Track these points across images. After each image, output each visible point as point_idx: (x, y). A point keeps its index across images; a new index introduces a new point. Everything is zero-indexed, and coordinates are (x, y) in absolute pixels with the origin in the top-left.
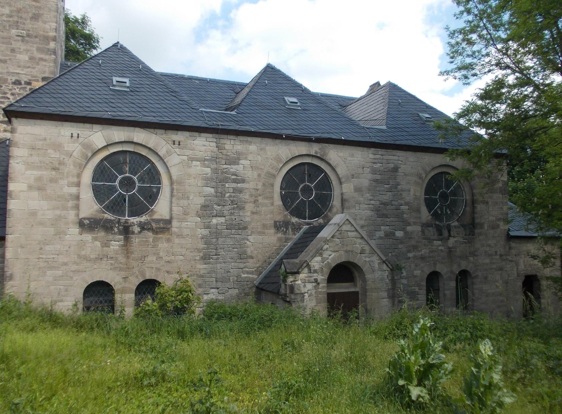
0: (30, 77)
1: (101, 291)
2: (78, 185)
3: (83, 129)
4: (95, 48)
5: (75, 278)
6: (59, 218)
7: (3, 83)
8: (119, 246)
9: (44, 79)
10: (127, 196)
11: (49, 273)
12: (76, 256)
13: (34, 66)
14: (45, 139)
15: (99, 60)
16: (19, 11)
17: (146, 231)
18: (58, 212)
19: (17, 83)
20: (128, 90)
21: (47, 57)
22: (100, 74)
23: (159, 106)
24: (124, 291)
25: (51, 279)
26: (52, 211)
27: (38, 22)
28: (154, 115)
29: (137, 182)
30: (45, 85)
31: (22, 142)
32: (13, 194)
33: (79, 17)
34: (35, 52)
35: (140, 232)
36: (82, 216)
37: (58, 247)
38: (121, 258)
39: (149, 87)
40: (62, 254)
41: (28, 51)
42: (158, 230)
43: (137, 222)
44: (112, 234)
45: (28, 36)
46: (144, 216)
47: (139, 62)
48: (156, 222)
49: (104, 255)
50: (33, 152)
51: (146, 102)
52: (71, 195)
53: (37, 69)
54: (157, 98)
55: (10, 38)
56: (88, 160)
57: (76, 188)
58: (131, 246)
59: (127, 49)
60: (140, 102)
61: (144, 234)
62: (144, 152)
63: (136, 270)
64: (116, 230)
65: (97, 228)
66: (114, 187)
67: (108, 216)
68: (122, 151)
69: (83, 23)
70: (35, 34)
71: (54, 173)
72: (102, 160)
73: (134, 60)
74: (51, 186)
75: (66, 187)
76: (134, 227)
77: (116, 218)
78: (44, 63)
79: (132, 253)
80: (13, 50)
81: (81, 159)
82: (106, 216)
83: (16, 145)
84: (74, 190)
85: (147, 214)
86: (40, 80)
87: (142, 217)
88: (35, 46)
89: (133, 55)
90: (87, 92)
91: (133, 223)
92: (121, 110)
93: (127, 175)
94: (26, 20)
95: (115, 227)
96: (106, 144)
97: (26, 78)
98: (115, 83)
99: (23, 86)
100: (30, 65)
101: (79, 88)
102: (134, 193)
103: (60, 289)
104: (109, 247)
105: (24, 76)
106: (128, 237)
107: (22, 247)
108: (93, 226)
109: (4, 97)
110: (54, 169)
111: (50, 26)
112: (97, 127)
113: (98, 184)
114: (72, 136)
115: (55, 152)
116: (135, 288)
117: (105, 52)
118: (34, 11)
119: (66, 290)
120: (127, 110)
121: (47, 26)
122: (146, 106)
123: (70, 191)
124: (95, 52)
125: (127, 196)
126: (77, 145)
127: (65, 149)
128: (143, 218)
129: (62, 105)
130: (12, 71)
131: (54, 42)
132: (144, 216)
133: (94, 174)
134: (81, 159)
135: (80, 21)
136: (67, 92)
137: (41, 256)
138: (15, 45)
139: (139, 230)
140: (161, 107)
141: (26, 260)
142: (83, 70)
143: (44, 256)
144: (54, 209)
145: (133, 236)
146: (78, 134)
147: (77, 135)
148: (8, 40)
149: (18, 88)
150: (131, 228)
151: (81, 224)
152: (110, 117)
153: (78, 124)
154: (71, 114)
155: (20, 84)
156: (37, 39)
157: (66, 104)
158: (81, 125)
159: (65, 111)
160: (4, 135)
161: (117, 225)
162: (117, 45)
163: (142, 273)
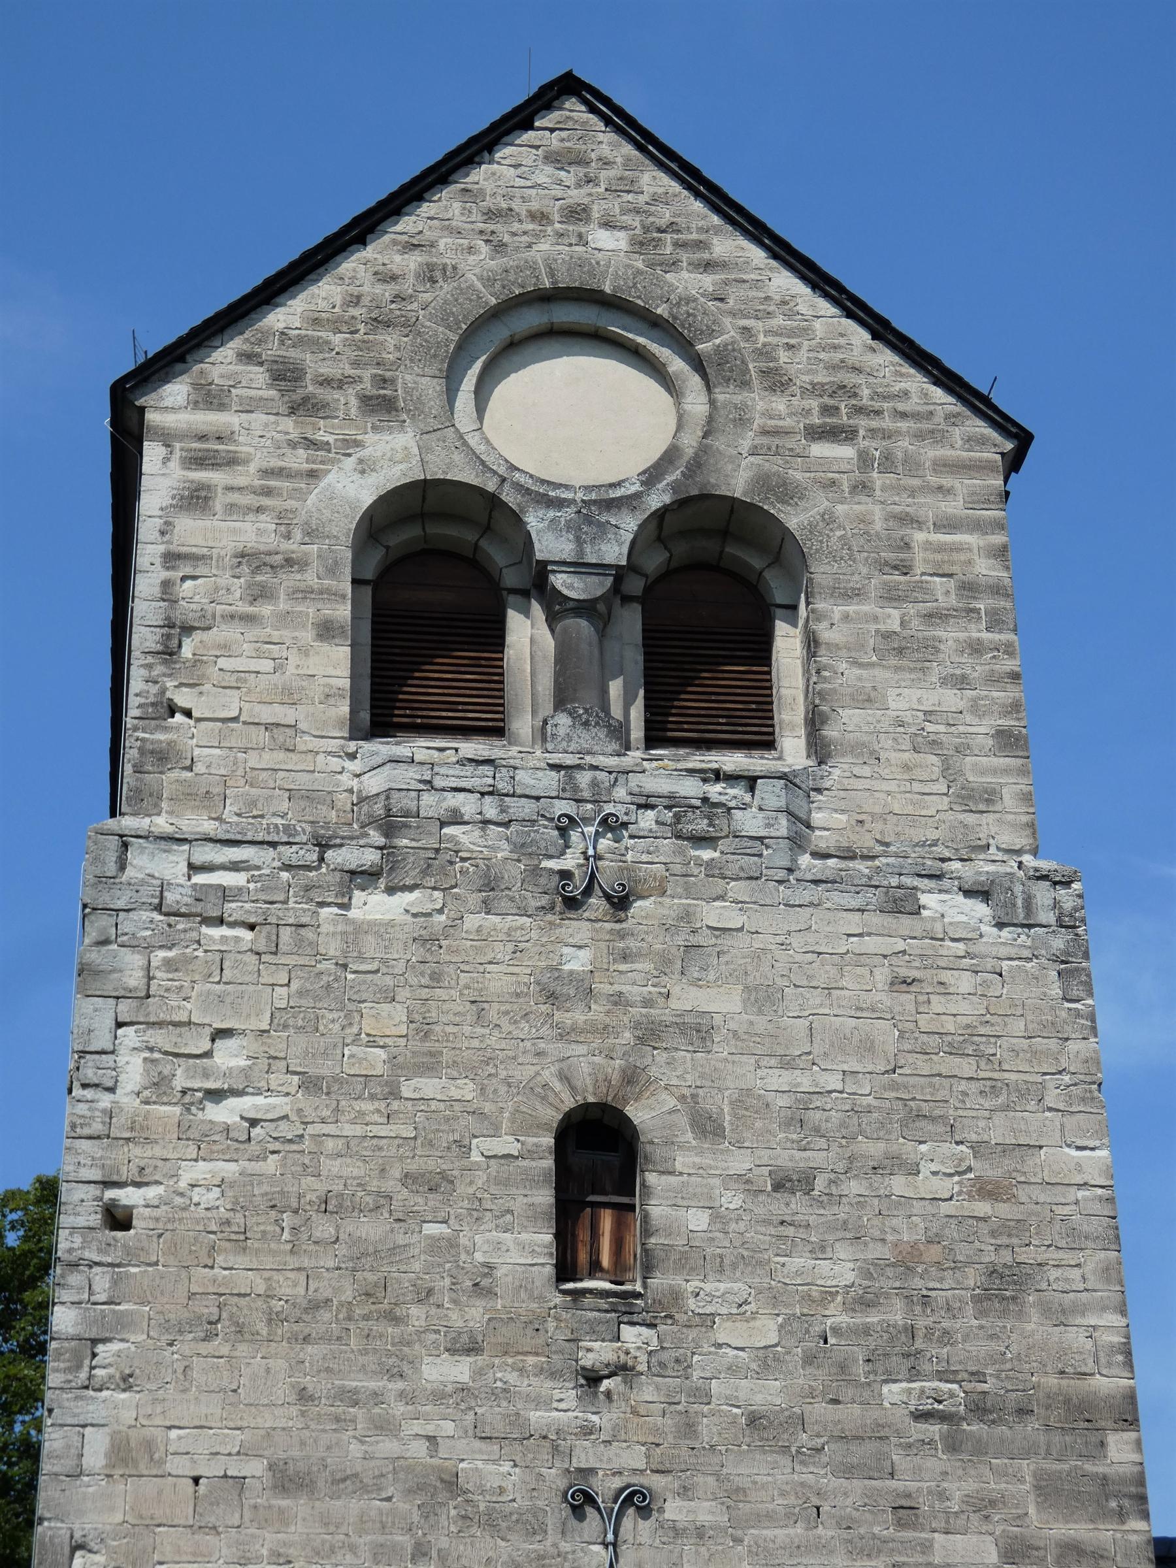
34: (1032, 1510)
41: (993, 1503)
45: (980, 1408)
88: (1026, 1467)
118: (989, 1257)
121: (1075, 1338)
148: (871, 1447)
156: (1032, 1425)
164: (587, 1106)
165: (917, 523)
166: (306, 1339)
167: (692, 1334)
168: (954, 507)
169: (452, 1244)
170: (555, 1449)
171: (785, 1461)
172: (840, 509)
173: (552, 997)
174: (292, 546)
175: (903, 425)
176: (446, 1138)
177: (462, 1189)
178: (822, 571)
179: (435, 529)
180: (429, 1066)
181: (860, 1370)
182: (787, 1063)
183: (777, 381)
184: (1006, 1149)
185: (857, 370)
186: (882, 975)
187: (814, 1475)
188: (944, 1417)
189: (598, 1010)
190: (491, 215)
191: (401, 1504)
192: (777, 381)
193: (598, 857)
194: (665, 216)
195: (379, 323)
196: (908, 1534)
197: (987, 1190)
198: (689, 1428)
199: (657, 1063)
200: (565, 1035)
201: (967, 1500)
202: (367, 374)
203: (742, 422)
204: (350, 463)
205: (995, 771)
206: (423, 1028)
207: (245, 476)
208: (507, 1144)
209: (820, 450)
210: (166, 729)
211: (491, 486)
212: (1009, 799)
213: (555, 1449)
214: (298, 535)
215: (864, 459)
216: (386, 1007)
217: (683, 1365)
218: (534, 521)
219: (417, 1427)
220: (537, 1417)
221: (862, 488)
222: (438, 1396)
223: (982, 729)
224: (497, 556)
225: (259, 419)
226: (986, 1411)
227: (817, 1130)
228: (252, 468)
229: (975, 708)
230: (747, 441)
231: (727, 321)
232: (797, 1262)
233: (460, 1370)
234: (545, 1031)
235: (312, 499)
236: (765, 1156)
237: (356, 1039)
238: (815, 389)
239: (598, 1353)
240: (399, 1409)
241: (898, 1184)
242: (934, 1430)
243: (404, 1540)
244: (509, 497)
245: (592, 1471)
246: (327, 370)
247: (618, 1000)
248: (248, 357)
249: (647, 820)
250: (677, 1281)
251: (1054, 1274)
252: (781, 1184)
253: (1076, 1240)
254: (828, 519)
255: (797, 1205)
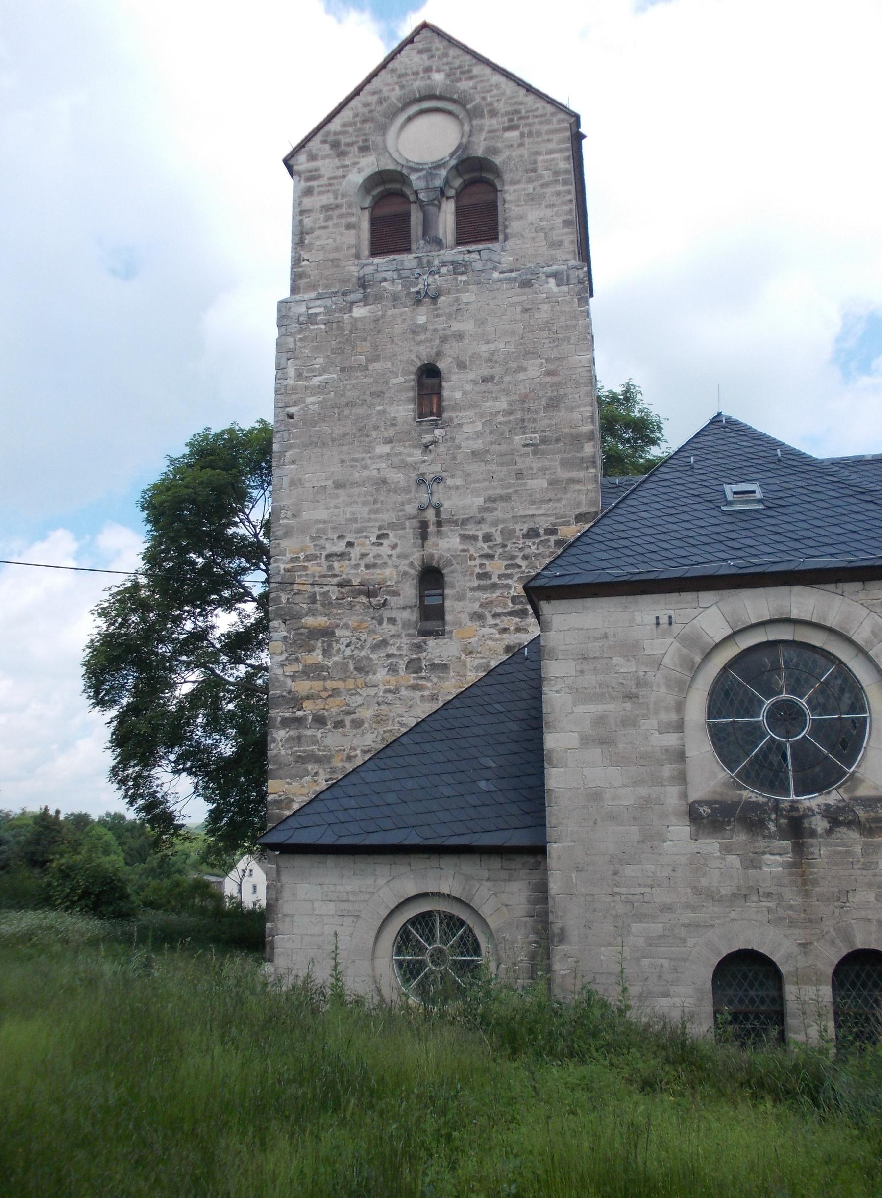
0: (552, 519)
1: (750, 975)
2: (680, 727)
3: (679, 606)
4: (654, 442)
5: (691, 942)
6: (646, 803)
7: (508, 540)
8: (781, 864)
9: (579, 518)
10: (788, 746)
11: (636, 927)
12: (689, 890)
13: (559, 496)
14: (605, 636)
15: (689, 457)
16: (524, 399)
17: (844, 830)
18: (643, 791)
19: (533, 533)
20: (762, 507)
21: (581, 474)
22: (695, 486)
23: (838, 530)
24: (803, 978)
25: (641, 942)
26: (632, 788)
27: (558, 411)
28: (833, 551)
29: (808, 711)
30: (592, 526)
31: (563, 647)
32: (554, 755)
33: (619, 390)
34: (559, 470)
35: (829, 832)
36: (693, 796)
37: (650, 867)
38: (792, 897)
39: (806, 492)
40: (659, 885)
41: (547, 469)
42: (873, 825)
43: (819, 805)
44: (764, 837)
45: (544, 441)
46: (834, 792)
47: (773, 444)
48: (865, 806)
49: (750, 888)
50: (585, 667)
51: (806, 526)
52: (667, 751)
53: (564, 502)
54: (830, 513)
55: (512, 452)
56: (695, 670)
57: (676, 735)
58: (810, 865)
59: (741, 423)
60: (792, 528)
61: (839, 835)
62: (817, 639)
63: (828, 926)
64: (772, 827)
65: (729, 823)
66: (757, 726)
67: (751, 795)
68: (768, 642)
69: (627, 399)
70: (555, 436)
71: (628, 705)
72: (724, 668)
73: (760, 442)
74: (625, 735)
75: (656, 734)
76: (814, 818)
77: (770, 799)
78: (577, 487)
79: (815, 882)
80: (520, 475)
81: (679, 670)
82: (745, 794)
83: (553, 656)
84: (671, 740)
85: (839, 787)
86: (572, 520)
87: (829, 793)
88: (558, 457)
89: (755, 432)
90: (675, 527)
91: (809, 809)
92: (753, 551)
93: (784, 696)
94: (536, 412)
95: (770, 819)
96: (729, 631)
97: (546, 522)
98: (730, 497)
99: (543, 539)
100: (551, 495)
101: (657, 521)
102: (804, 736)
103: (662, 966)
104: (760, 868)
105: (543, 518)
106: (802, 844)
107: (578, 869)
108: (721, 819)
109: (512, 565)
110: (630, 697)
111: (581, 414)
112: (707, 597)
113: (721, 723)
114: (658, 624)
115: (628, 660)
116: (830, 971)
117: (696, 440)
118: (549, 394)
119: (675, 970)
120: (769, 550)
121: (576, 415)
122: (808, 534)
123: (664, 743)
124: (655, 452)
125: (788, 746)
126: (669, 640)
127: (647, 652)
128: (833, 797)
129: (631, 560)
130: (521, 513)
131: (592, 443)
132: (834, 792)
133: (710, 701)
134: (679, 670)
135: (622, 397)
136: (637, 533)
137: (617, 890)
138: (522, 463)
139: (827, 826)
140: (842, 531)
141: (589, 899)
142: (659, 483)
143: (624, 890)
144: (636, 783)
145: (813, 841)
146: (670, 617)
147: (667, 621)
148: (509, 457)
149: (534, 544)
150: (806, 824)
151: (694, 815)
152: (734, 571)
153: (667, 595)
154: (652, 576)
155: (538, 535)
156: (560, 444)
157: (639, 557)
158: (674, 597)
159: (640, 573)
160: (516, 638)
161: (773, 816)
162: (718, 419)
163: (846, 935)
164: (425, 365)
165: (538, 153)
166: (343, 445)
167: (455, 430)
168: (552, 146)
169: (384, 412)
170: (415, 468)
171: (483, 464)
172: (514, 154)
173: (414, 332)
174: (339, 201)
175: (536, 120)
176: (382, 381)
177: (387, 395)
178: (507, 177)
179: (388, 186)
180: (377, 359)
181: (507, 435)
182: (488, 342)
183: (493, 113)
184: (556, 359)
185: (521, 104)
186: (519, 309)
187: (493, 467)
188: (532, 445)
189: (428, 335)
190: (400, 76)
191: (370, 489)
192: (493, 113)
193: (428, 285)
194: (457, 63)
195: (365, 121)
196: (520, 481)
197: (549, 373)
198: (454, 458)
199: (447, 348)
200: (418, 344)
201: (539, 469)
202: (360, 139)
203: (481, 130)
204: (355, 170)
205: (562, 235)
206: (375, 347)
207: (324, 181)
208: (401, 379)
209: (508, 135)
210: (301, 267)
211: (399, 169)
212: (567, 243)
213: (415, 468)
214: (339, 197)
215: (522, 135)
216: (364, 343)
217: (453, 439)
218: (413, 177)
219: (374, 466)
220: (409, 460)
221: (521, 145)
222: (381, 457)
223: (559, 221)
224: (408, 192)
225: (327, 161)
226: (546, 442)
227: (496, 362)
228: (326, 178)
229: (557, 214)
230: (483, 135)
231: (477, 96)
232: (488, 404)
233: (386, 449)
234: (412, 343)
235: (344, 184)
236: (480, 372)
237: (356, 355)
238: (507, 113)
239: (428, 438)
240: (369, 462)
241: (521, 375)
242: (529, 449)
243: (371, 499)
244: (405, 171)
245: (425, 474)
246: (348, 140)
247: (435, 330)
248: (324, 142)
249: (444, 270)
250: (453, 415)
251: (570, 396)
252: (484, 380)
253: (578, 384)
254: (509, 158)
255: (490, 386)
